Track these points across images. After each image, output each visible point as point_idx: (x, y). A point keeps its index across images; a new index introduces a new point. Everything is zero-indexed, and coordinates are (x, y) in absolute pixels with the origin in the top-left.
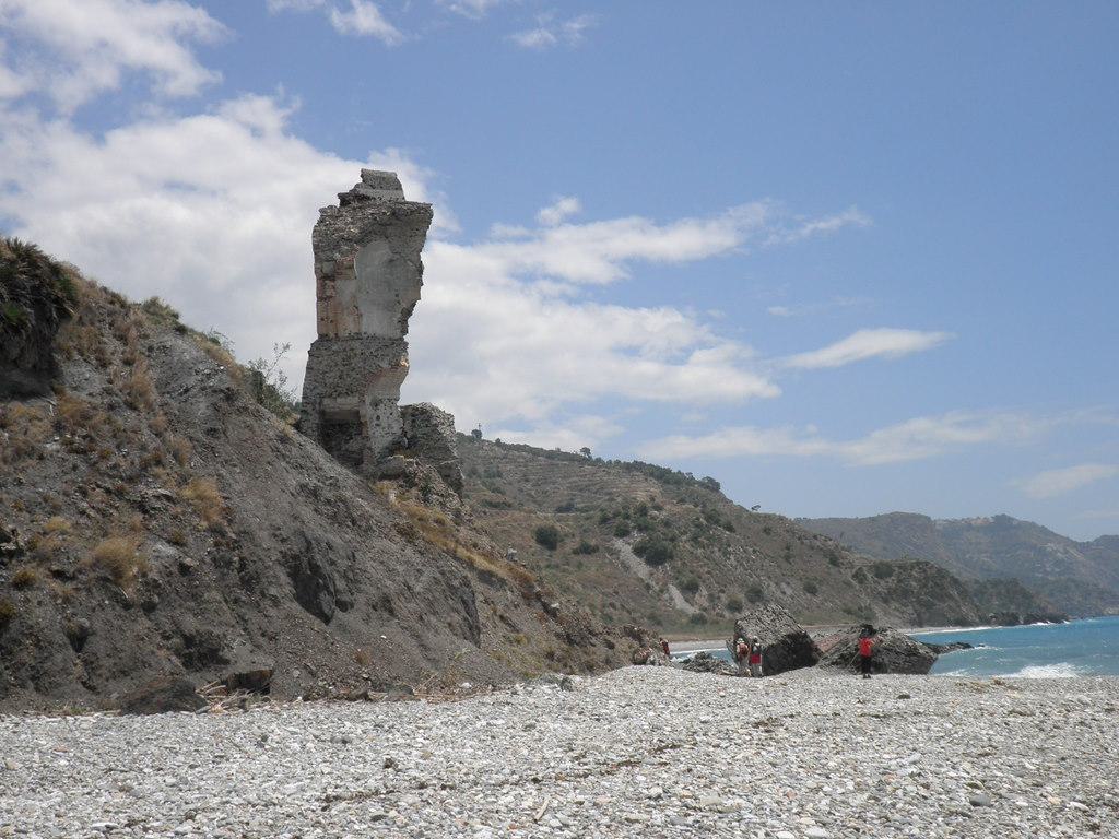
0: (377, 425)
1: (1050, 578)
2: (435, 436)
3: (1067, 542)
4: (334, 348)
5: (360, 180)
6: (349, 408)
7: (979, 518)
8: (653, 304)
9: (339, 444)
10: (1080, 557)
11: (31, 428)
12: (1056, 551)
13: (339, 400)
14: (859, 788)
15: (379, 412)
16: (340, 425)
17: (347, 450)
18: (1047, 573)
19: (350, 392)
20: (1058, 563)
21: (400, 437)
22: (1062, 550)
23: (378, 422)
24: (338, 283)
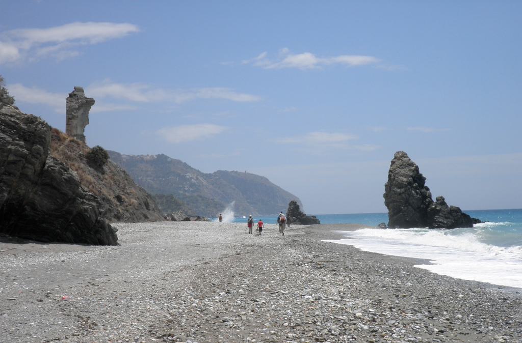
1: (187, 194)
3: (198, 173)
5: (74, 90)
7: (148, 155)
10: (205, 182)
12: (192, 178)
14: (27, 330)
18: (186, 191)
20: (192, 185)
22: (195, 178)
24: (72, 120)
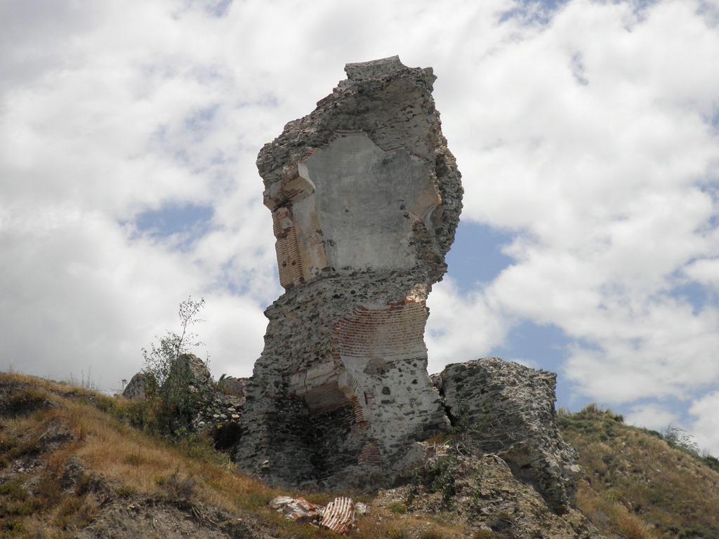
0: (384, 402)
2: (497, 405)
4: (299, 299)
6: (322, 380)
8: (398, 487)
9: (335, 443)
11: (439, 397)
13: (310, 373)
15: (387, 382)
16: (333, 414)
17: (346, 451)
19: (320, 357)
21: (434, 416)
23: (387, 398)
